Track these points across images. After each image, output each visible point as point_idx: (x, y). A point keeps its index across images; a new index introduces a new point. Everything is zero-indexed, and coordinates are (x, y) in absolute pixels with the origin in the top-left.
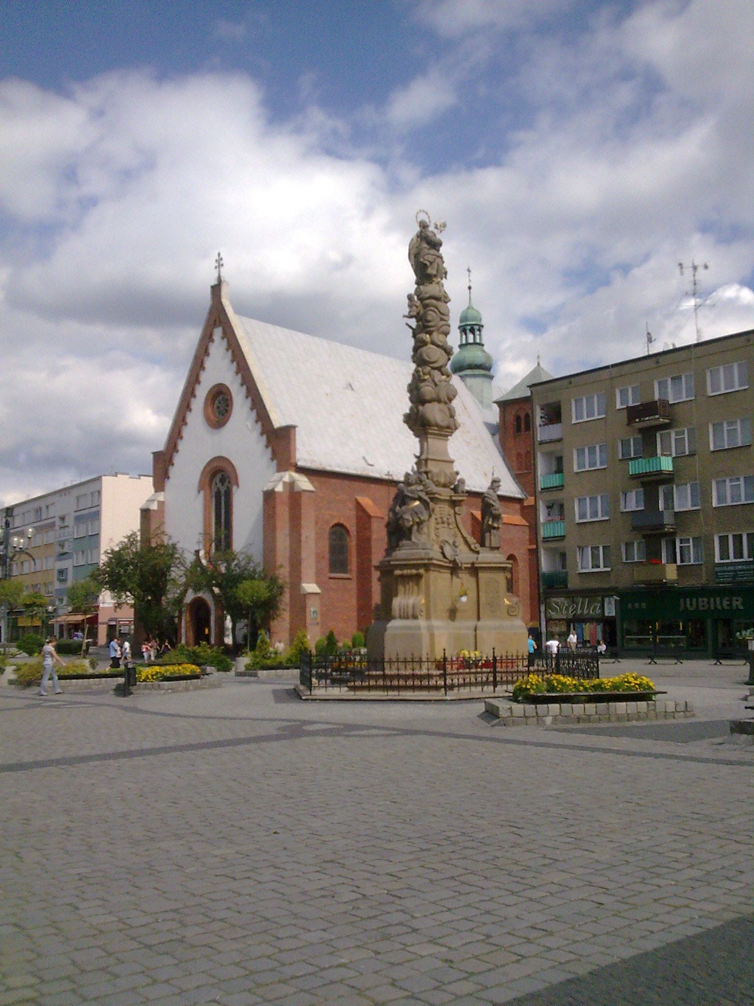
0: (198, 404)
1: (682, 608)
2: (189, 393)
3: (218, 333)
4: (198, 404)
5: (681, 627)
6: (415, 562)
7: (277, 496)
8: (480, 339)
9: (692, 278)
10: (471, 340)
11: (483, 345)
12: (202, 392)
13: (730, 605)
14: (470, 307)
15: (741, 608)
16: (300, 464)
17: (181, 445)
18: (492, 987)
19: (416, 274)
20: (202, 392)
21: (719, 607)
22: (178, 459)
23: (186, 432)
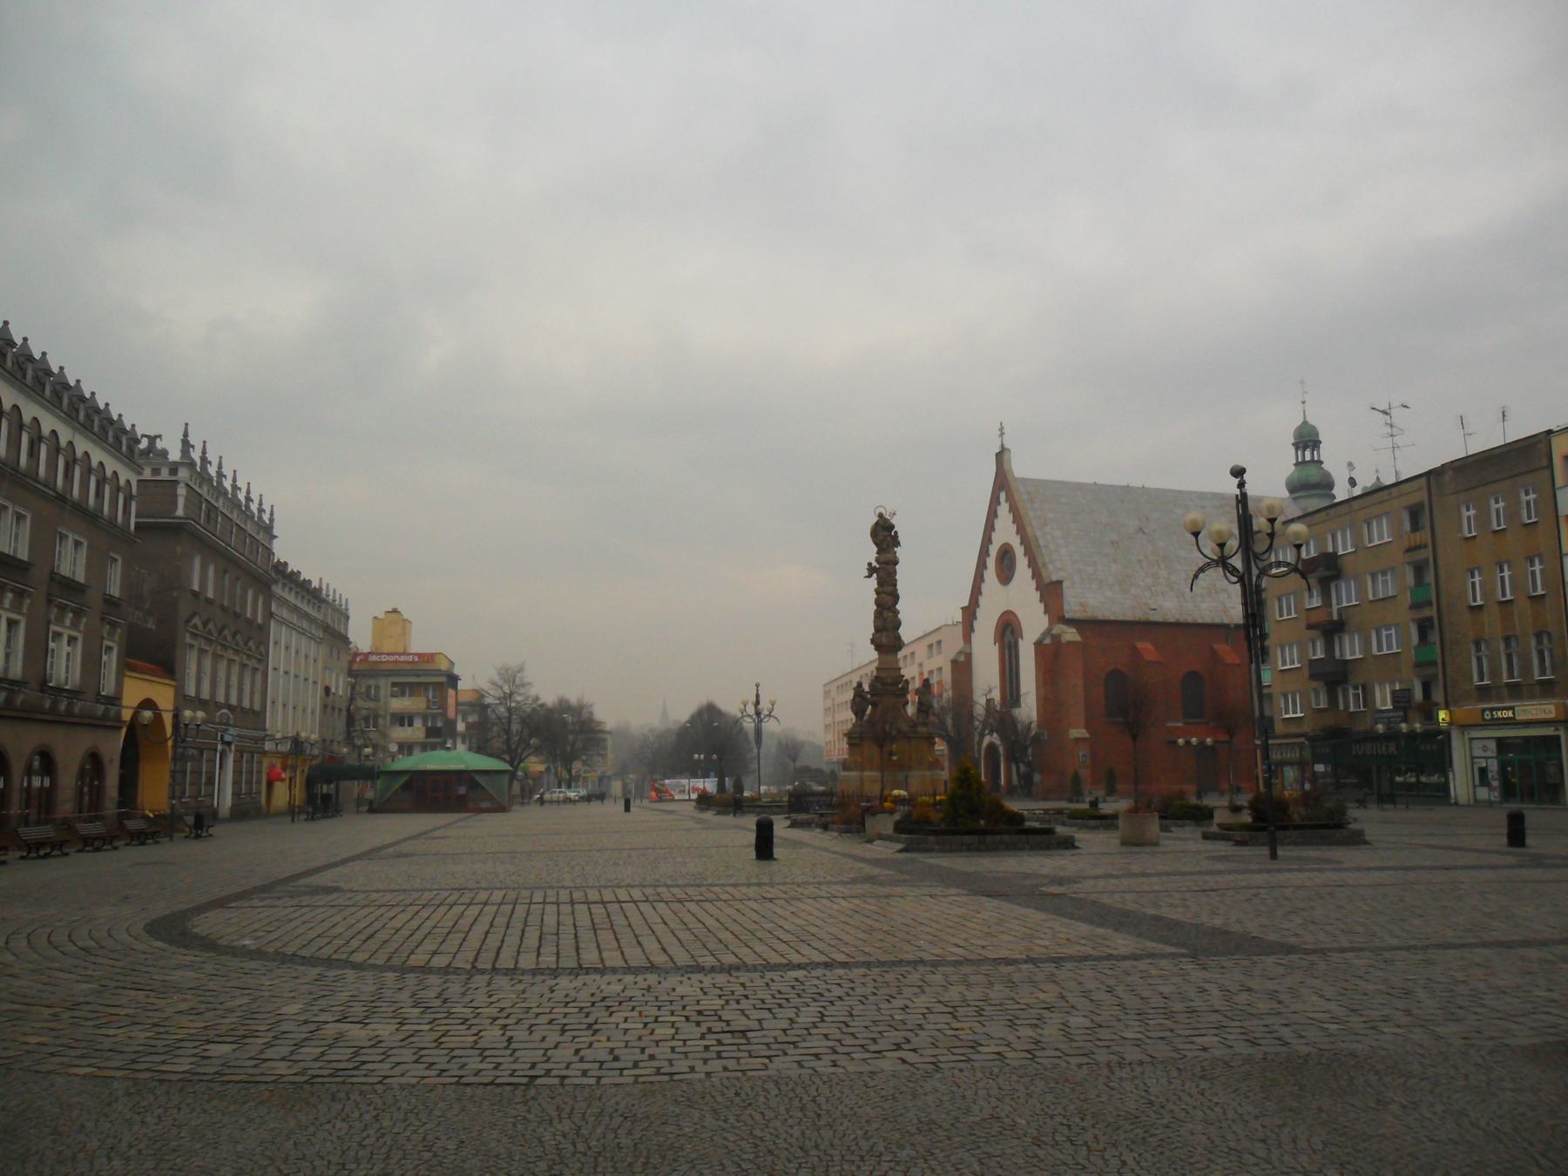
0: (991, 562)
1: (1354, 752)
2: (984, 552)
3: (1003, 496)
4: (991, 562)
5: (181, 502)
6: (1193, 720)
7: (388, 646)
8: (1319, 455)
9: (1238, 492)
10: (1308, 457)
11: (1322, 463)
12: (994, 550)
13: (1387, 750)
14: (1305, 422)
15: (1395, 753)
16: (1068, 616)
17: (982, 600)
18: (1209, 1138)
19: (693, 720)
20: (994, 550)
21: (1380, 753)
22: (979, 612)
23: (984, 588)
